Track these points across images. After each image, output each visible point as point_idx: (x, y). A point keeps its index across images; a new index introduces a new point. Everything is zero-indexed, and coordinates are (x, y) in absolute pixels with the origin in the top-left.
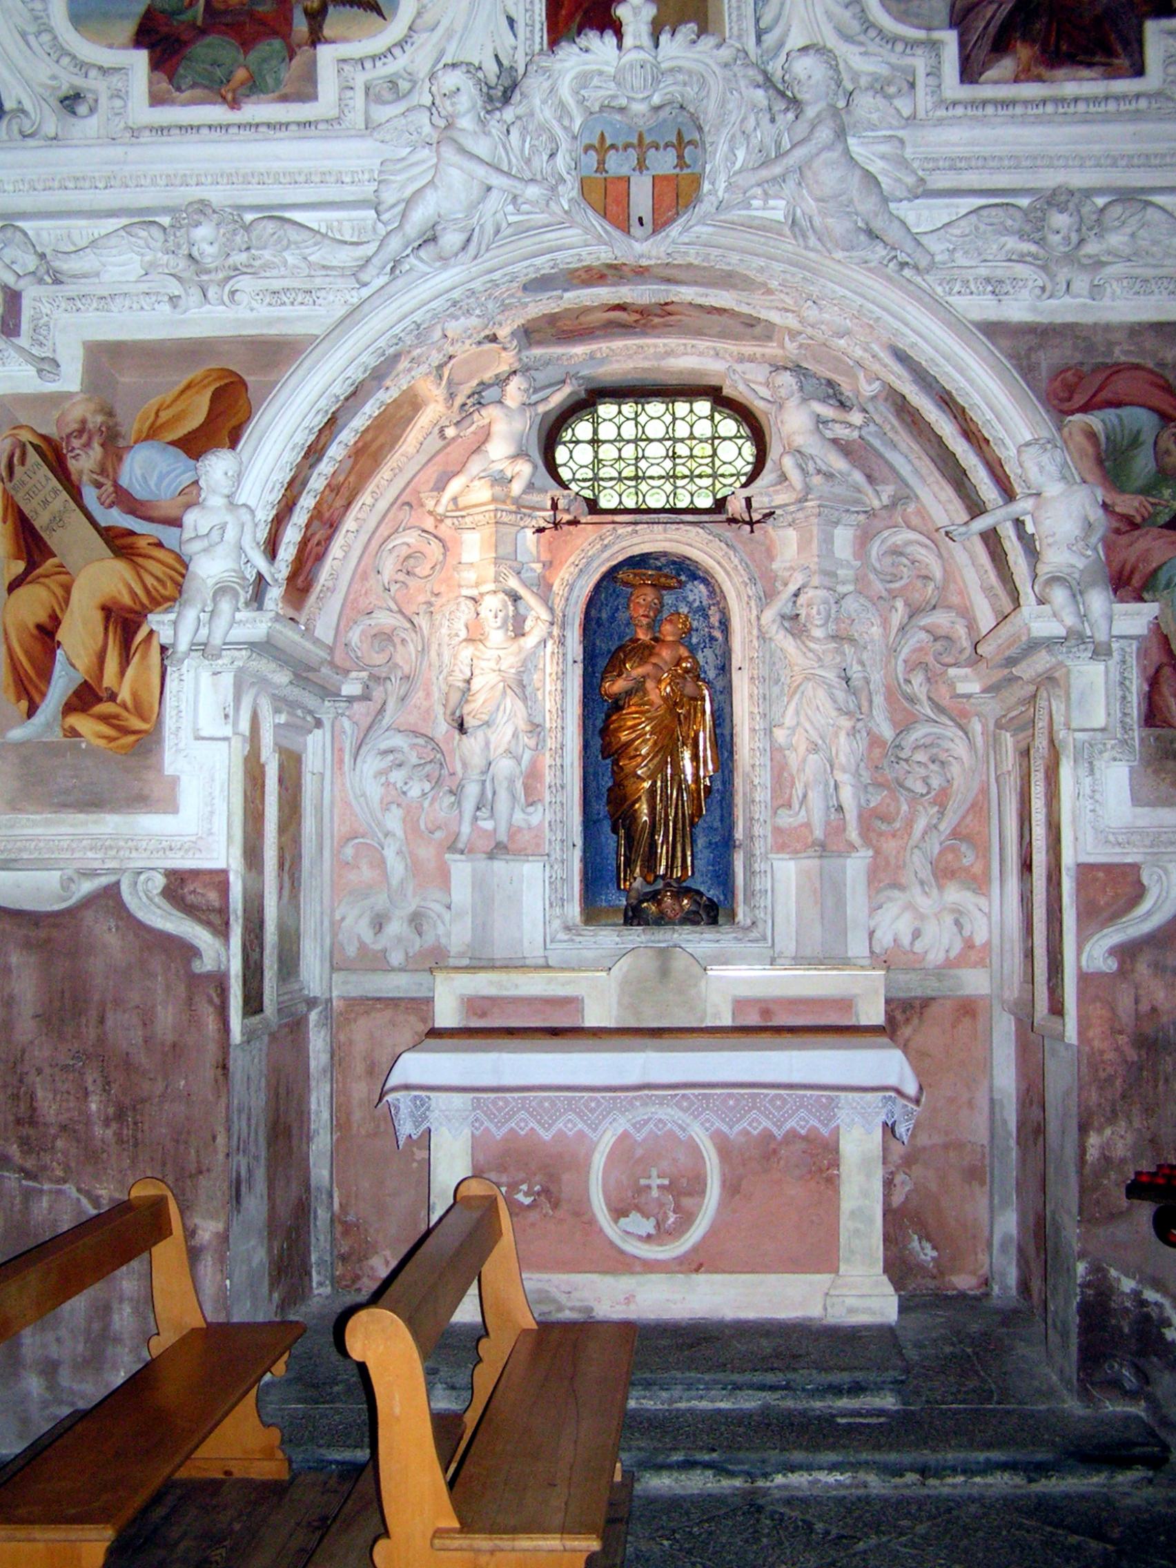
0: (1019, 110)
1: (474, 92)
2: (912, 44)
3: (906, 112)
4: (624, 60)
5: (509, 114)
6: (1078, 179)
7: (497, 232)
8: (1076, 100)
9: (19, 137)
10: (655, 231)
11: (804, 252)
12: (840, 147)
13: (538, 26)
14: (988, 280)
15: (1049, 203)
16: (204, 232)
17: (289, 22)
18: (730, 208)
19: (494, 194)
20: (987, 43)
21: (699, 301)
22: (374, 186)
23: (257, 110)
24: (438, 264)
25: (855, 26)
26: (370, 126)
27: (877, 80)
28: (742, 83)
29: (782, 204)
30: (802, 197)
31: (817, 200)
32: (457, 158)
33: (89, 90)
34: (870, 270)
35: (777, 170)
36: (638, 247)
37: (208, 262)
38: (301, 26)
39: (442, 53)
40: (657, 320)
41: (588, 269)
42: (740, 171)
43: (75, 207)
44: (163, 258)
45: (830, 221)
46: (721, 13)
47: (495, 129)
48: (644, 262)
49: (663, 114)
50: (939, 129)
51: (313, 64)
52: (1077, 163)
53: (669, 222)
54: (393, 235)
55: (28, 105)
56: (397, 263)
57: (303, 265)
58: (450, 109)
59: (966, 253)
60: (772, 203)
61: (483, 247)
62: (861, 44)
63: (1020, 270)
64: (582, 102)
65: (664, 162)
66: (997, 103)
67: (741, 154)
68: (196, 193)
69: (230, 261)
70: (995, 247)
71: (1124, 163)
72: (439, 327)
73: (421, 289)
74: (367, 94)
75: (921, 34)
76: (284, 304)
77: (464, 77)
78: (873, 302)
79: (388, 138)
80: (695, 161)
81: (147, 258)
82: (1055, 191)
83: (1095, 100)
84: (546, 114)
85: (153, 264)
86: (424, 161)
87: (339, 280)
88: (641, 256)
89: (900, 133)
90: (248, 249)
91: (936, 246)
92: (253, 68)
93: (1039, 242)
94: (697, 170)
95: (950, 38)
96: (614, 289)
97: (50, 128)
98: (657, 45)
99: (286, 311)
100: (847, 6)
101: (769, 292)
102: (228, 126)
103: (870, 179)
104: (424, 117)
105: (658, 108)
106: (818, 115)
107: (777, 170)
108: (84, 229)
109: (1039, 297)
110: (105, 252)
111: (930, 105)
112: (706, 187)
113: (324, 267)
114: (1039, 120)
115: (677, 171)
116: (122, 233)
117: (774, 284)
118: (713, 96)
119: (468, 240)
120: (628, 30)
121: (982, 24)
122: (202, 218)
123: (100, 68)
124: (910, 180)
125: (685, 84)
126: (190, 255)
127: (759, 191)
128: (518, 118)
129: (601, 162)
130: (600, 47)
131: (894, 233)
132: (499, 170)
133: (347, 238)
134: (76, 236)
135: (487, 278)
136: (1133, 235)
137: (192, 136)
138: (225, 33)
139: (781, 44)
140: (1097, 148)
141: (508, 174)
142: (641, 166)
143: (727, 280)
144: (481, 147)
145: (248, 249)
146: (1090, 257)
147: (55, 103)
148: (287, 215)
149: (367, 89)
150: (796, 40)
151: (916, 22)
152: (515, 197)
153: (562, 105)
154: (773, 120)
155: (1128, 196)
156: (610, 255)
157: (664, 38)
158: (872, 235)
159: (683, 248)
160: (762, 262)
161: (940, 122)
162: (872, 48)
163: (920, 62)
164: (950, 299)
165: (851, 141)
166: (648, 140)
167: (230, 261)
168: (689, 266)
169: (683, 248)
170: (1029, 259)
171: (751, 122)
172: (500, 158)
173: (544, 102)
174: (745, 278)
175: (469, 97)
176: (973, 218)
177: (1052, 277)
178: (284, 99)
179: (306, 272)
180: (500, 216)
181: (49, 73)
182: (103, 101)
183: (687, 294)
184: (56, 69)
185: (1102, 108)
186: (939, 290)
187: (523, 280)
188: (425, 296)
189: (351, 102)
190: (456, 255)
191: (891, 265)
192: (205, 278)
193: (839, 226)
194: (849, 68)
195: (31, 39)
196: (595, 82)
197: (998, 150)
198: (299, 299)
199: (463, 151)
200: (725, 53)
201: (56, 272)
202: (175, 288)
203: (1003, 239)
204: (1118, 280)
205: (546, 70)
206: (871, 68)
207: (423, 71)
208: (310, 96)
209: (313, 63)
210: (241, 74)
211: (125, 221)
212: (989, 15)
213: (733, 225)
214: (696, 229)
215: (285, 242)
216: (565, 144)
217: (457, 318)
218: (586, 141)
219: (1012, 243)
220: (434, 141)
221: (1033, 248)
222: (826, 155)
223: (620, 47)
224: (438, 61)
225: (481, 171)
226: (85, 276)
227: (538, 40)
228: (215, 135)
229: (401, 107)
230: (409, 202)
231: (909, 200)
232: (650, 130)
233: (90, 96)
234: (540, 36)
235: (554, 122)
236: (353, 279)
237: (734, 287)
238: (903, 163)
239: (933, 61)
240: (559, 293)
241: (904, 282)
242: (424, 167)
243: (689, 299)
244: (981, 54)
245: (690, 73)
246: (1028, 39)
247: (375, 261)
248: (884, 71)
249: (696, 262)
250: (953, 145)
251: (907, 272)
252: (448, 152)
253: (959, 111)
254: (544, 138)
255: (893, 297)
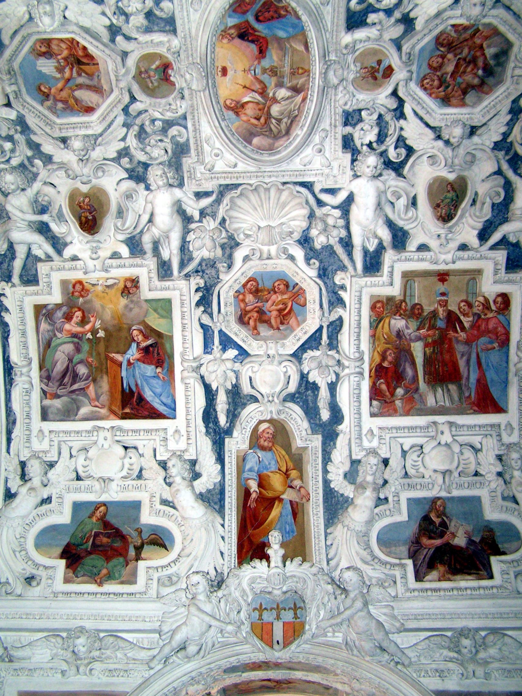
0: (442, 593)
1: (206, 584)
2: (393, 565)
3: (393, 594)
4: (270, 573)
5: (220, 593)
6: (473, 624)
7: (213, 646)
8: (466, 589)
9: (4, 594)
10: (284, 647)
11: (351, 657)
12: (366, 610)
13: (233, 556)
14: (437, 670)
15: (460, 635)
16: (81, 641)
17: (127, 551)
18: (317, 636)
19: (213, 629)
20: (425, 565)
21: (304, 678)
22: (159, 623)
23: (110, 587)
24: (186, 660)
25: (369, 558)
26: (159, 597)
27: (379, 580)
28: (322, 582)
29: (341, 635)
30: (350, 632)
31: (357, 633)
32: (197, 613)
33: (39, 575)
34: (382, 665)
35: (339, 620)
36: (277, 654)
37: (81, 655)
38: (132, 552)
39: (192, 566)
40: (284, 685)
41: (254, 663)
42: (322, 620)
43: (24, 627)
44: (61, 652)
45: (363, 643)
46: (311, 552)
47: (214, 600)
48: (279, 661)
49: (287, 595)
50: (408, 602)
51: (136, 569)
52: (471, 616)
53: (291, 643)
54: (166, 646)
55: (11, 581)
56: (167, 659)
57: (124, 658)
58: (195, 591)
59: (425, 657)
60: (336, 634)
61: (207, 652)
62: (372, 565)
63: (451, 665)
64: (252, 589)
65: (288, 616)
66: (432, 590)
67: (322, 613)
68: (79, 623)
69: (92, 654)
70: (438, 654)
71: (491, 616)
72: (185, 689)
73: (178, 671)
74: (158, 582)
75: (397, 561)
76: (114, 676)
77: (201, 577)
78: (385, 681)
79: (167, 602)
80: (302, 616)
81: (54, 652)
82: (462, 629)
83: (474, 589)
84: (237, 594)
85: (56, 655)
86: (182, 613)
87: (140, 666)
88: (278, 658)
89: (392, 604)
90: (100, 649)
91: (411, 654)
92: (110, 569)
93: (459, 652)
94: (303, 619)
95: (409, 563)
96: (265, 672)
97: (18, 591)
98: (285, 566)
99: (115, 680)
100: (365, 550)
101: (336, 675)
102: (97, 594)
103: (380, 624)
104: (182, 594)
105: (285, 593)
106: (355, 596)
107: (339, 620)
108: (27, 637)
109: (461, 679)
110: (35, 648)
111: (403, 591)
112: (307, 627)
113: (134, 659)
114: (451, 598)
115: (294, 620)
116: (44, 639)
117: (338, 671)
118: (309, 587)
119: (200, 649)
120: (272, 560)
121: (422, 557)
122: (81, 635)
123: (44, 566)
124: (398, 625)
125: (297, 582)
126: (73, 651)
127: (330, 629)
128: (225, 595)
129: (261, 615)
130: (260, 566)
131: (392, 648)
132: (215, 618)
133: (145, 646)
134: (23, 639)
135: (207, 667)
136: (500, 649)
137: (80, 598)
138: (99, 554)
139: (338, 565)
140: (478, 610)
141: (219, 620)
142: (278, 618)
143: (317, 669)
144: (208, 608)
145: (100, 649)
146: (482, 659)
147: (22, 580)
148: (119, 634)
149: (159, 580)
150: (344, 564)
151: (394, 556)
152: (222, 631)
153: (244, 590)
154: (336, 598)
155: (494, 631)
156: (264, 657)
157: (288, 563)
158: (383, 649)
159: (297, 654)
160: (333, 661)
161: (409, 599)
162: (377, 567)
163: (397, 573)
164: (419, 679)
165: (370, 607)
166: (281, 606)
167: (92, 654)
168: (300, 663)
169: (297, 654)
170: (454, 660)
171: (326, 598)
172: (216, 613)
173: (236, 589)
174: (325, 669)
175: (203, 586)
176: (427, 641)
177: (466, 669)
178: (122, 583)
179: (126, 661)
180: (215, 638)
181: (22, 567)
182: (44, 580)
183: (299, 675)
184: (25, 566)
185: (478, 592)
186: (414, 675)
187: (224, 668)
188: (179, 675)
189: (151, 586)
190: (194, 656)
191: (392, 663)
192: (79, 662)
193: (367, 646)
194: (367, 575)
195: (17, 554)
196: (258, 581)
197: (436, 611)
198: (121, 674)
199: (199, 609)
200: (314, 570)
201: (11, 656)
202: (65, 666)
203: (441, 651)
204: (497, 670)
205: (237, 576)
206: (377, 575)
207: (183, 573)
208: (134, 582)
209: (136, 568)
210: (104, 571)
211: (46, 634)
212: (425, 553)
213: (320, 644)
214: (303, 646)
215: (117, 647)
216: (244, 608)
217: (193, 685)
218: (254, 606)
219: (446, 652)
220: (187, 604)
221: (456, 655)
222: (360, 614)
223: (269, 566)
224: (190, 569)
225: (207, 619)
226: (24, 659)
227: (233, 561)
228: (90, 597)
229: (173, 589)
230: (174, 632)
231: (398, 633)
232: (282, 602)
233: (38, 578)
234: (234, 560)
235: (240, 598)
236: (147, 666)
237: (320, 672)
238: (394, 617)
239: (403, 572)
240: (240, 673)
241: (399, 672)
242: (182, 615)
243: (300, 677)
244: (423, 569)
245: (299, 578)
246: (442, 563)
247: (157, 657)
248: (382, 576)
249: (303, 661)
250: (415, 609)
251: (399, 667)
252: (193, 609)
253: (416, 593)
254: (235, 604)
255: (393, 678)
